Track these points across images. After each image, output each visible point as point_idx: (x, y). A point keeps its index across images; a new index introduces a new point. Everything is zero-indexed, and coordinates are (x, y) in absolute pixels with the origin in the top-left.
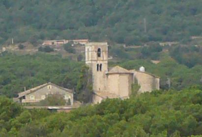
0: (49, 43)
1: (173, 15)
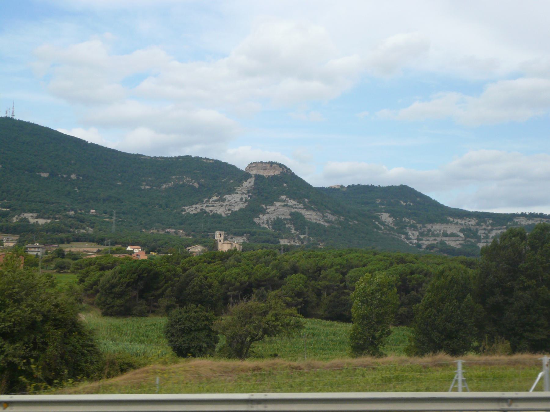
0: (169, 230)
1: (212, 223)
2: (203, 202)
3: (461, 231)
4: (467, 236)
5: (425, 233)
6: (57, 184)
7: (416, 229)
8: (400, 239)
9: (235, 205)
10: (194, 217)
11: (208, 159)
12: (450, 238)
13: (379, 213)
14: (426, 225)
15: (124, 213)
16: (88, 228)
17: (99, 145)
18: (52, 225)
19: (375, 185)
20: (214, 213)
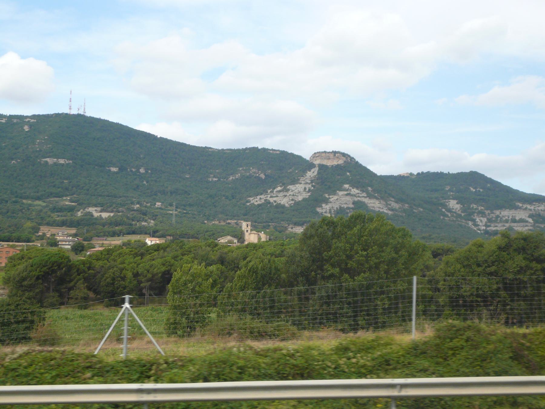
0: (230, 221)
1: (275, 214)
2: (267, 192)
3: (530, 216)
4: (536, 222)
5: (494, 219)
6: (126, 178)
7: (484, 216)
8: (467, 225)
9: (298, 195)
10: (258, 207)
11: (275, 150)
12: (519, 224)
13: (447, 200)
14: (494, 212)
15: (190, 205)
16: (149, 220)
17: (168, 139)
18: (115, 218)
19: (445, 172)
20: (277, 203)
